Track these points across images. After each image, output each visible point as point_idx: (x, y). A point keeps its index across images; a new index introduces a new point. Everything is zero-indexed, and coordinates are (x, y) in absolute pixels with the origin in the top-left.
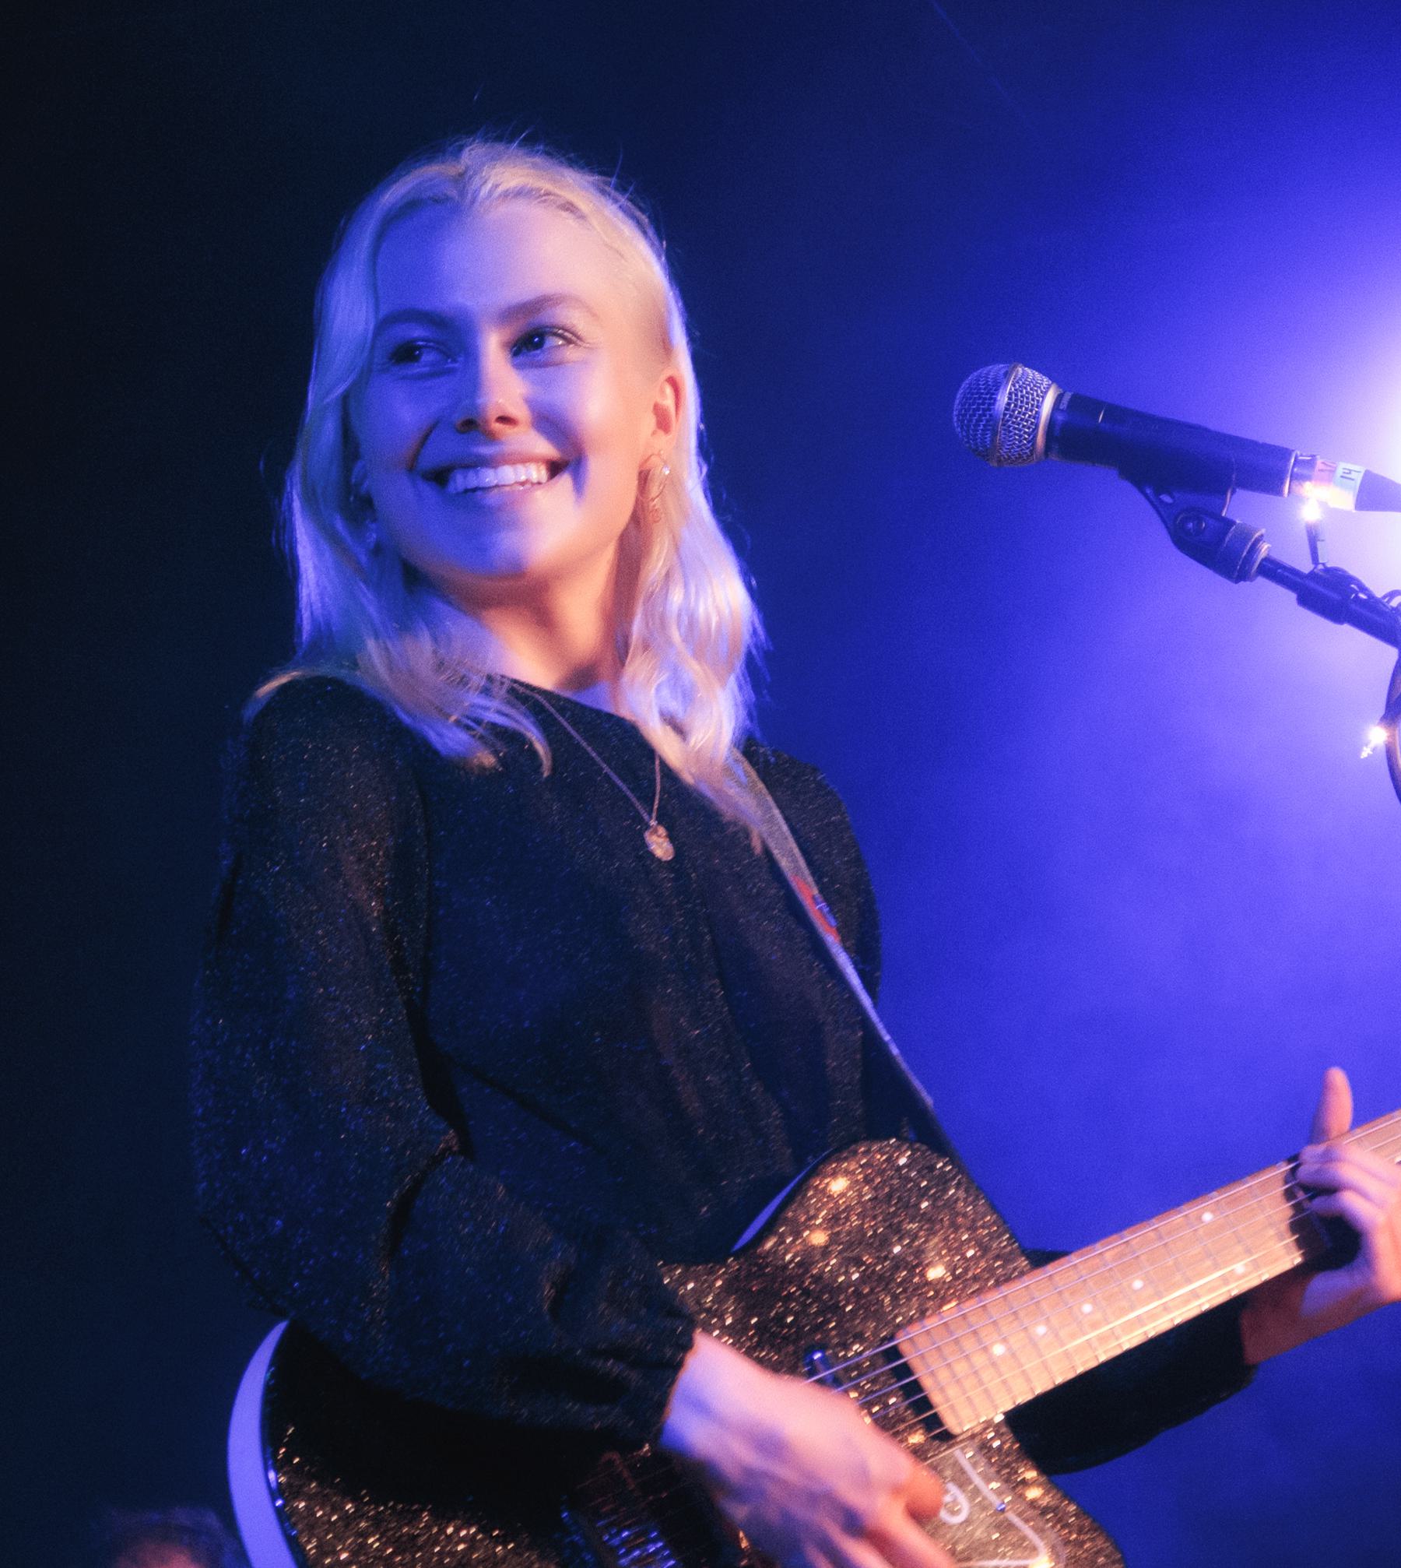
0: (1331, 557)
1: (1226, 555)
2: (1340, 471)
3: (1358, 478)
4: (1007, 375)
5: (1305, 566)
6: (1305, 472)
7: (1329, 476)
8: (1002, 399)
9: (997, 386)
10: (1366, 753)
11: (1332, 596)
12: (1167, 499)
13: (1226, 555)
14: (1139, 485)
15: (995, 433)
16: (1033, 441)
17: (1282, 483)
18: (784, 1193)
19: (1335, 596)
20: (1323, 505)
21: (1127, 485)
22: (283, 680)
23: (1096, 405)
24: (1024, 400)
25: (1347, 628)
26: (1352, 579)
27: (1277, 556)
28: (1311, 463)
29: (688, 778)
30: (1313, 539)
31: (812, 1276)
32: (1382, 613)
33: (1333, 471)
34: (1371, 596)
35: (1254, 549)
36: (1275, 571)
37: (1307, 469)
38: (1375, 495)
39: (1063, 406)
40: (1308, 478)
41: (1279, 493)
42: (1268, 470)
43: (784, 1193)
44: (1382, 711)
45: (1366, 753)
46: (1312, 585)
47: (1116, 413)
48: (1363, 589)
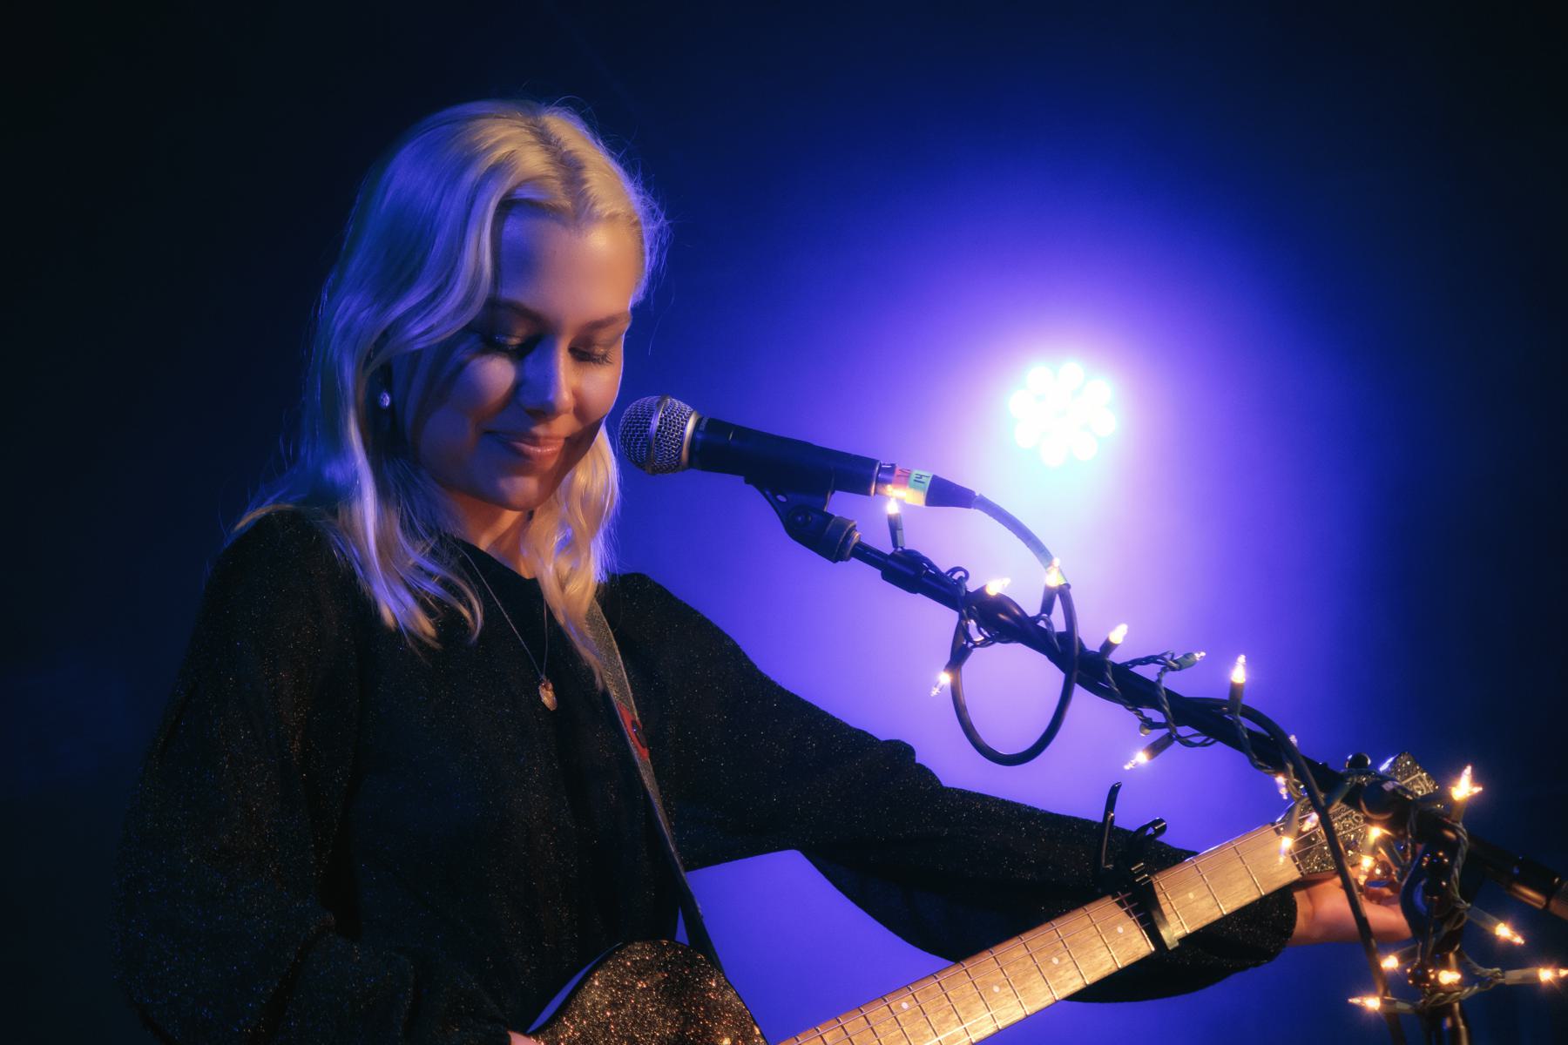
0: (910, 542)
1: (831, 542)
2: (913, 477)
3: (928, 481)
4: (659, 404)
5: (888, 549)
6: (886, 477)
7: (904, 480)
8: (655, 423)
9: (650, 413)
10: (935, 692)
11: (911, 572)
12: (781, 498)
13: (831, 542)
14: (760, 486)
15: (649, 449)
16: (679, 455)
17: (869, 486)
18: (582, 974)
19: (911, 573)
20: (900, 501)
21: (751, 489)
22: (260, 513)
23: (728, 427)
24: (672, 424)
25: (920, 598)
26: (925, 560)
27: (868, 541)
28: (891, 470)
29: (561, 620)
30: (894, 526)
31: (1147, 913)
32: (945, 585)
33: (908, 477)
34: (938, 571)
35: (849, 536)
36: (866, 554)
37: (889, 474)
38: (944, 494)
39: (702, 428)
40: (889, 482)
41: (867, 493)
42: (861, 475)
43: (582, 974)
44: (947, 658)
45: (935, 692)
46: (891, 562)
47: (743, 433)
48: (931, 565)
